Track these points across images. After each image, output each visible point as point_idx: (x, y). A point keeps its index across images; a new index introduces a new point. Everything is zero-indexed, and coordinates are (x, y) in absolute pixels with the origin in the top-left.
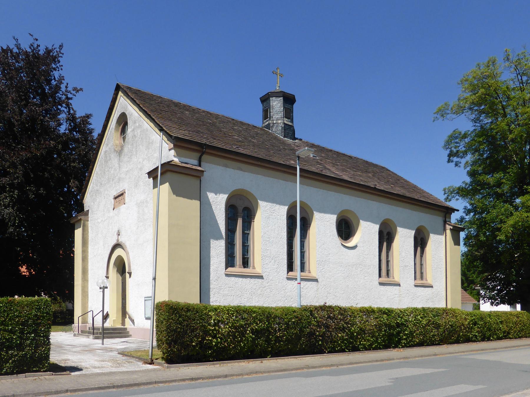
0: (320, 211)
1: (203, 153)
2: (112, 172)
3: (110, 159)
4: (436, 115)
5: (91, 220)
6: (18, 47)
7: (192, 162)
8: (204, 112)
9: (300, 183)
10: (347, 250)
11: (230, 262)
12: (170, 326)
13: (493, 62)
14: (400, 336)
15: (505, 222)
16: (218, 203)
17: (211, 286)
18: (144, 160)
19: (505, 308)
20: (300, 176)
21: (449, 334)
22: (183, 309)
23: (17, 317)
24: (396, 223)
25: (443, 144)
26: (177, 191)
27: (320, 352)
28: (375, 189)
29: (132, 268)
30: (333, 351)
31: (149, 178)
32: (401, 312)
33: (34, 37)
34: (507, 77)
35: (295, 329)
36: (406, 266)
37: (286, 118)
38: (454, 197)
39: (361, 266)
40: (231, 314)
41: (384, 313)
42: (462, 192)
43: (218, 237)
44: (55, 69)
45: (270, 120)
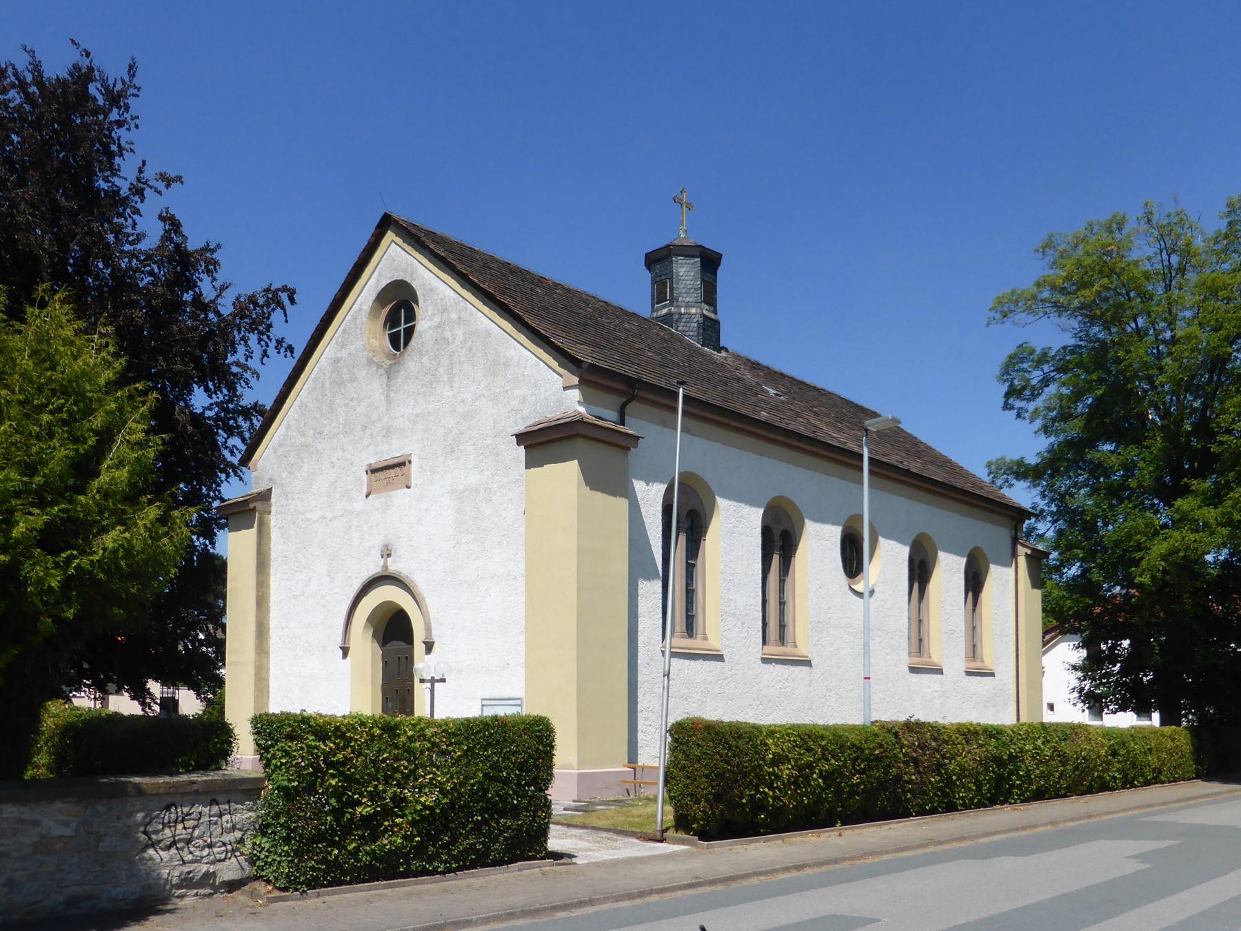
0: (817, 519)
3: (354, 379)
4: (993, 314)
6: (36, 68)
7: (609, 417)
9: (870, 486)
16: (650, 495)
19: (1125, 720)
20: (871, 472)
24: (935, 538)
25: (997, 371)
26: (595, 480)
28: (908, 472)
31: (519, 444)
34: (1142, 252)
36: (952, 632)
43: (650, 577)
44: (120, 124)
45: (671, 304)
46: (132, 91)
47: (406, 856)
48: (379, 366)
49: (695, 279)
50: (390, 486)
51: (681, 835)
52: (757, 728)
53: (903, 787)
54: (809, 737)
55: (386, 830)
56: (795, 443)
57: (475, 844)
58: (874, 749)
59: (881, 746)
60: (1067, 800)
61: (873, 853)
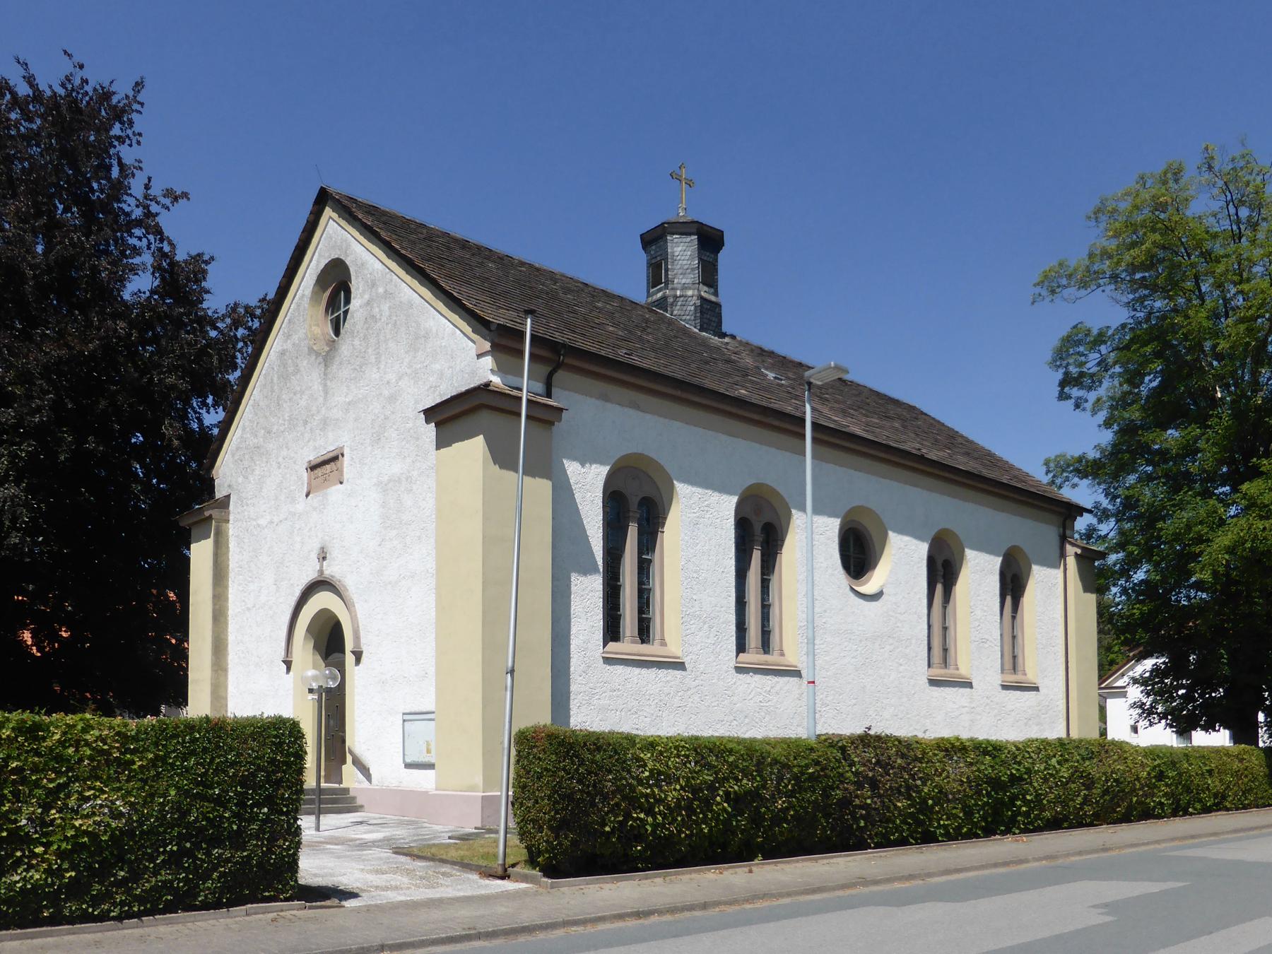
1: (557, 366)
2: (303, 403)
3: (297, 371)
4: (1038, 289)
5: (236, 520)
8: (522, 264)
10: (861, 601)
11: (612, 631)
12: (560, 788)
13: (1175, 174)
14: (1015, 805)
15: (1208, 540)
16: (588, 482)
17: (573, 688)
18: (400, 379)
21: (1112, 799)
22: (585, 744)
23: (233, 764)
24: (962, 537)
26: (502, 456)
27: (860, 845)
29: (363, 641)
30: (885, 843)
31: (427, 421)
32: (1018, 749)
33: (77, 59)
34: (1204, 207)
35: (814, 792)
36: (984, 641)
37: (704, 284)
38: (1067, 479)
39: (891, 641)
40: (685, 756)
41: (986, 753)
42: (1087, 469)
43: (588, 569)
44: (121, 140)
46: (136, 106)
47: (54, 899)
48: (318, 354)
49: (691, 258)
50: (326, 482)
51: (528, 871)
52: (631, 739)
53: (853, 814)
54: (711, 751)
55: (18, 862)
56: (776, 423)
57: (171, 882)
58: (807, 766)
59: (817, 763)
60: (1092, 830)
61: (765, 896)
